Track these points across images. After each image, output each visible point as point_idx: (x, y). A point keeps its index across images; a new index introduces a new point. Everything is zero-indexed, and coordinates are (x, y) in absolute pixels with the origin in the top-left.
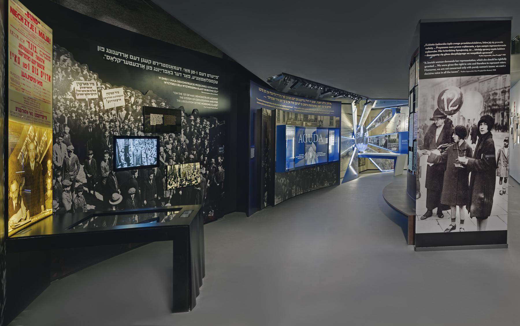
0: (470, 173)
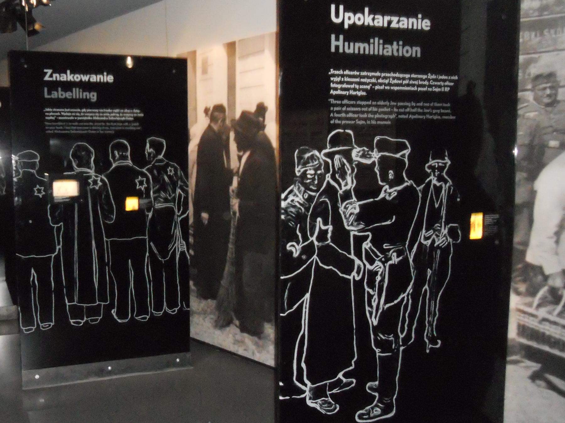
0: (110, 79)
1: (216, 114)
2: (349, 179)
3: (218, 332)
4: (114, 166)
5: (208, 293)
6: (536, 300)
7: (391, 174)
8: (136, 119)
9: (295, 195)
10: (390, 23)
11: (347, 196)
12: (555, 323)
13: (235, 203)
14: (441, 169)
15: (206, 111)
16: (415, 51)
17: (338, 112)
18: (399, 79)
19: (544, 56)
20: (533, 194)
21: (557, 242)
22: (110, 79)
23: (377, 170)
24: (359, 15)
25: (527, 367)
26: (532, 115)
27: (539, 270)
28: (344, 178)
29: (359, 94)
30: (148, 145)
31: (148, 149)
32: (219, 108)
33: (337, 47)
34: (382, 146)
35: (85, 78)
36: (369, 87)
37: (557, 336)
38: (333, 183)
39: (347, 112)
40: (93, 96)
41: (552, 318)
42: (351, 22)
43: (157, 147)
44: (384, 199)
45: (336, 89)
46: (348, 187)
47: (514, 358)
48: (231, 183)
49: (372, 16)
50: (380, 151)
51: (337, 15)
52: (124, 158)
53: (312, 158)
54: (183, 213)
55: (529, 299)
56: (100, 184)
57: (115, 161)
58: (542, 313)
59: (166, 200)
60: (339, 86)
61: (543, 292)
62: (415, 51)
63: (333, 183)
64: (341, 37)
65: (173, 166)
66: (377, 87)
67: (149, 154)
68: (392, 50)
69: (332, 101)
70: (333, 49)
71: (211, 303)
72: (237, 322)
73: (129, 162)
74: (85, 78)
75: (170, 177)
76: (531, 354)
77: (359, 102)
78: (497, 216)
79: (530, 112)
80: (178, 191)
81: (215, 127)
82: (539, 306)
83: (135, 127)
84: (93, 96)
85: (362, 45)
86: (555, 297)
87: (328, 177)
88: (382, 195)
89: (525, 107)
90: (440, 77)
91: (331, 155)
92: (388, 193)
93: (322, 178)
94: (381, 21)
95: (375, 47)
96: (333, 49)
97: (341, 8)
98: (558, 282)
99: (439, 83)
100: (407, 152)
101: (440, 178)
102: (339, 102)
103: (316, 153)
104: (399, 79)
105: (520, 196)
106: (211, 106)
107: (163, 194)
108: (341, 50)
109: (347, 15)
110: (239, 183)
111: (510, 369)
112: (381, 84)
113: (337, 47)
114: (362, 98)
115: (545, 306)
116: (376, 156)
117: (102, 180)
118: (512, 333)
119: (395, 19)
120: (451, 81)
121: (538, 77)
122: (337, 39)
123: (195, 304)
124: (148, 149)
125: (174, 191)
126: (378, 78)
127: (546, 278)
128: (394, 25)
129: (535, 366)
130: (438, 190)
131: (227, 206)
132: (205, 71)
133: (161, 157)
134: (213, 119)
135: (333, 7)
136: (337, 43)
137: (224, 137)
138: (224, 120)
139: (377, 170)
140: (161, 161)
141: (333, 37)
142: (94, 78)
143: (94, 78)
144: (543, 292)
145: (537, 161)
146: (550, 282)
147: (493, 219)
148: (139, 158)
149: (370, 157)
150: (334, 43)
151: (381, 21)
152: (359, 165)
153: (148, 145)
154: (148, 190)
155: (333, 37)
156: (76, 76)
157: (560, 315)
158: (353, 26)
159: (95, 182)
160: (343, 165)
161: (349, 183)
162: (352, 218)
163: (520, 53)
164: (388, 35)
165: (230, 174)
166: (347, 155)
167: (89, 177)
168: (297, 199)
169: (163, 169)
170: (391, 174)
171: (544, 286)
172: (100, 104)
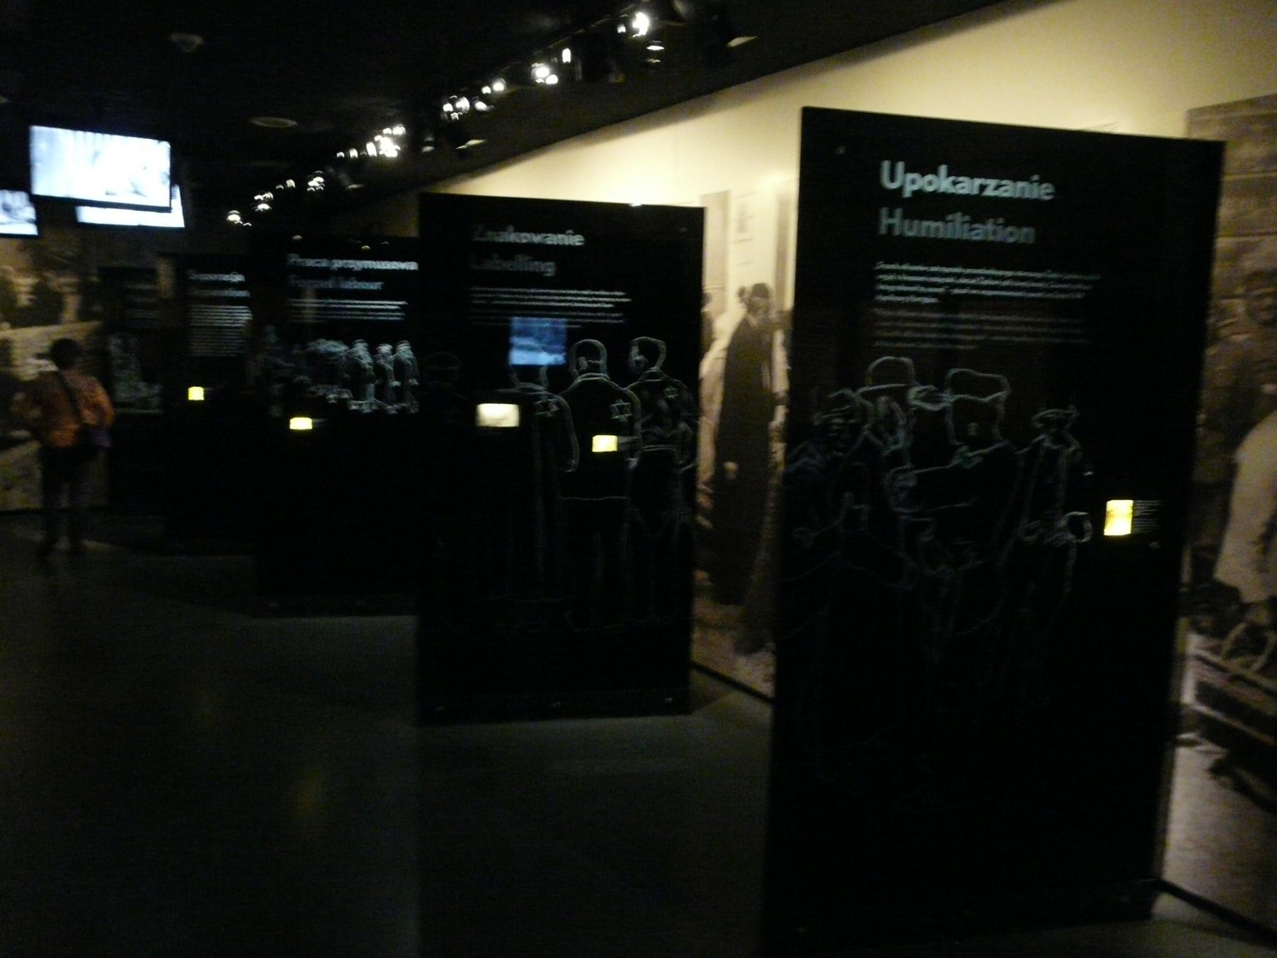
0: (576, 240)
1: (757, 299)
2: (901, 434)
3: (741, 661)
4: (579, 380)
5: (725, 595)
6: (1227, 645)
7: (973, 428)
8: (618, 307)
9: (811, 456)
10: (983, 188)
11: (896, 458)
12: (1253, 684)
13: (778, 449)
14: (1060, 423)
15: (741, 293)
16: (1022, 235)
17: (889, 329)
18: (994, 278)
19: (1267, 239)
20: (1231, 470)
21: (1265, 551)
22: (576, 240)
23: (949, 421)
24: (929, 177)
25: (1207, 753)
26: (1241, 338)
27: (1232, 593)
28: (892, 432)
29: (927, 300)
30: (635, 350)
31: (636, 356)
32: (760, 290)
33: (890, 227)
34: (957, 385)
35: (537, 239)
36: (941, 290)
37: (1255, 706)
38: (873, 438)
39: (904, 329)
40: (549, 269)
41: (1249, 674)
42: (915, 187)
43: (650, 352)
44: (957, 467)
45: (885, 293)
46: (900, 446)
47: (1185, 736)
48: (771, 417)
49: (952, 178)
50: (955, 392)
51: (892, 179)
52: (594, 368)
53: (843, 400)
54: (688, 463)
55: (1214, 642)
56: (555, 408)
57: (582, 373)
58: (1235, 665)
59: (661, 440)
60: (892, 288)
61: (1238, 630)
62: (1022, 235)
63: (873, 438)
64: (898, 212)
65: (674, 385)
66: (956, 291)
67: (637, 362)
68: (985, 231)
69: (878, 311)
70: (883, 230)
71: (733, 611)
72: (771, 645)
73: (603, 376)
74: (537, 239)
75: (669, 401)
76: (1212, 731)
77: (924, 315)
78: (1155, 503)
79: (1238, 333)
80: (683, 426)
81: (754, 321)
82: (1232, 654)
83: (616, 319)
84: (549, 269)
85: (933, 225)
86: (1253, 642)
87: (866, 431)
88: (956, 461)
89: (1232, 324)
90: (1068, 277)
91: (871, 396)
92: (966, 457)
93: (856, 430)
94: (968, 186)
95: (955, 228)
96: (883, 230)
97: (900, 166)
98: (1263, 617)
99: (1065, 286)
100: (1002, 395)
101: (1058, 439)
102: (889, 313)
103: (848, 392)
104: (994, 278)
105: (1205, 472)
106: (749, 283)
107: (658, 430)
108: (897, 232)
109: (910, 176)
110: (788, 416)
111: (1183, 753)
112: (963, 286)
113: (890, 227)
114: (930, 307)
115: (1240, 655)
116: (948, 399)
117: (558, 404)
118: (1188, 696)
119: (992, 183)
120: (1086, 283)
121: (1257, 274)
122: (891, 215)
123: (703, 607)
124: (636, 356)
125: (675, 426)
126: (959, 276)
127: (1245, 608)
128: (989, 192)
129: (1218, 752)
130: (1053, 456)
131: (766, 454)
132: (742, 228)
133: (655, 369)
134: (751, 308)
135: (886, 165)
136: (892, 222)
137: (767, 337)
138: (767, 311)
139: (949, 421)
140: (654, 375)
141: (884, 211)
142: (554, 239)
143: (554, 239)
144: (1238, 630)
145: (1242, 416)
146: (1251, 616)
147: (1151, 507)
148: (620, 370)
149: (939, 402)
150: (885, 221)
151: (968, 186)
152: (920, 412)
153: (635, 350)
154: (632, 421)
155: (884, 211)
156: (523, 235)
157: (1263, 671)
158: (918, 194)
159: (546, 406)
160: (892, 413)
161: (901, 440)
162: (903, 496)
163: (1221, 232)
164: (977, 207)
165: (773, 401)
166: (900, 396)
167: (537, 398)
168: (812, 461)
169: (658, 389)
170: (973, 428)
171: (1240, 621)
172: (560, 282)
